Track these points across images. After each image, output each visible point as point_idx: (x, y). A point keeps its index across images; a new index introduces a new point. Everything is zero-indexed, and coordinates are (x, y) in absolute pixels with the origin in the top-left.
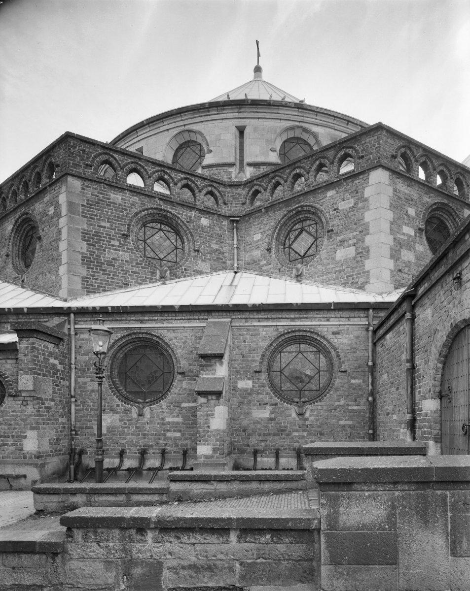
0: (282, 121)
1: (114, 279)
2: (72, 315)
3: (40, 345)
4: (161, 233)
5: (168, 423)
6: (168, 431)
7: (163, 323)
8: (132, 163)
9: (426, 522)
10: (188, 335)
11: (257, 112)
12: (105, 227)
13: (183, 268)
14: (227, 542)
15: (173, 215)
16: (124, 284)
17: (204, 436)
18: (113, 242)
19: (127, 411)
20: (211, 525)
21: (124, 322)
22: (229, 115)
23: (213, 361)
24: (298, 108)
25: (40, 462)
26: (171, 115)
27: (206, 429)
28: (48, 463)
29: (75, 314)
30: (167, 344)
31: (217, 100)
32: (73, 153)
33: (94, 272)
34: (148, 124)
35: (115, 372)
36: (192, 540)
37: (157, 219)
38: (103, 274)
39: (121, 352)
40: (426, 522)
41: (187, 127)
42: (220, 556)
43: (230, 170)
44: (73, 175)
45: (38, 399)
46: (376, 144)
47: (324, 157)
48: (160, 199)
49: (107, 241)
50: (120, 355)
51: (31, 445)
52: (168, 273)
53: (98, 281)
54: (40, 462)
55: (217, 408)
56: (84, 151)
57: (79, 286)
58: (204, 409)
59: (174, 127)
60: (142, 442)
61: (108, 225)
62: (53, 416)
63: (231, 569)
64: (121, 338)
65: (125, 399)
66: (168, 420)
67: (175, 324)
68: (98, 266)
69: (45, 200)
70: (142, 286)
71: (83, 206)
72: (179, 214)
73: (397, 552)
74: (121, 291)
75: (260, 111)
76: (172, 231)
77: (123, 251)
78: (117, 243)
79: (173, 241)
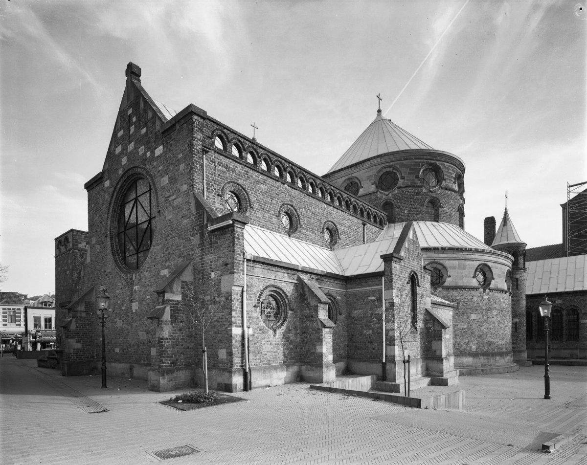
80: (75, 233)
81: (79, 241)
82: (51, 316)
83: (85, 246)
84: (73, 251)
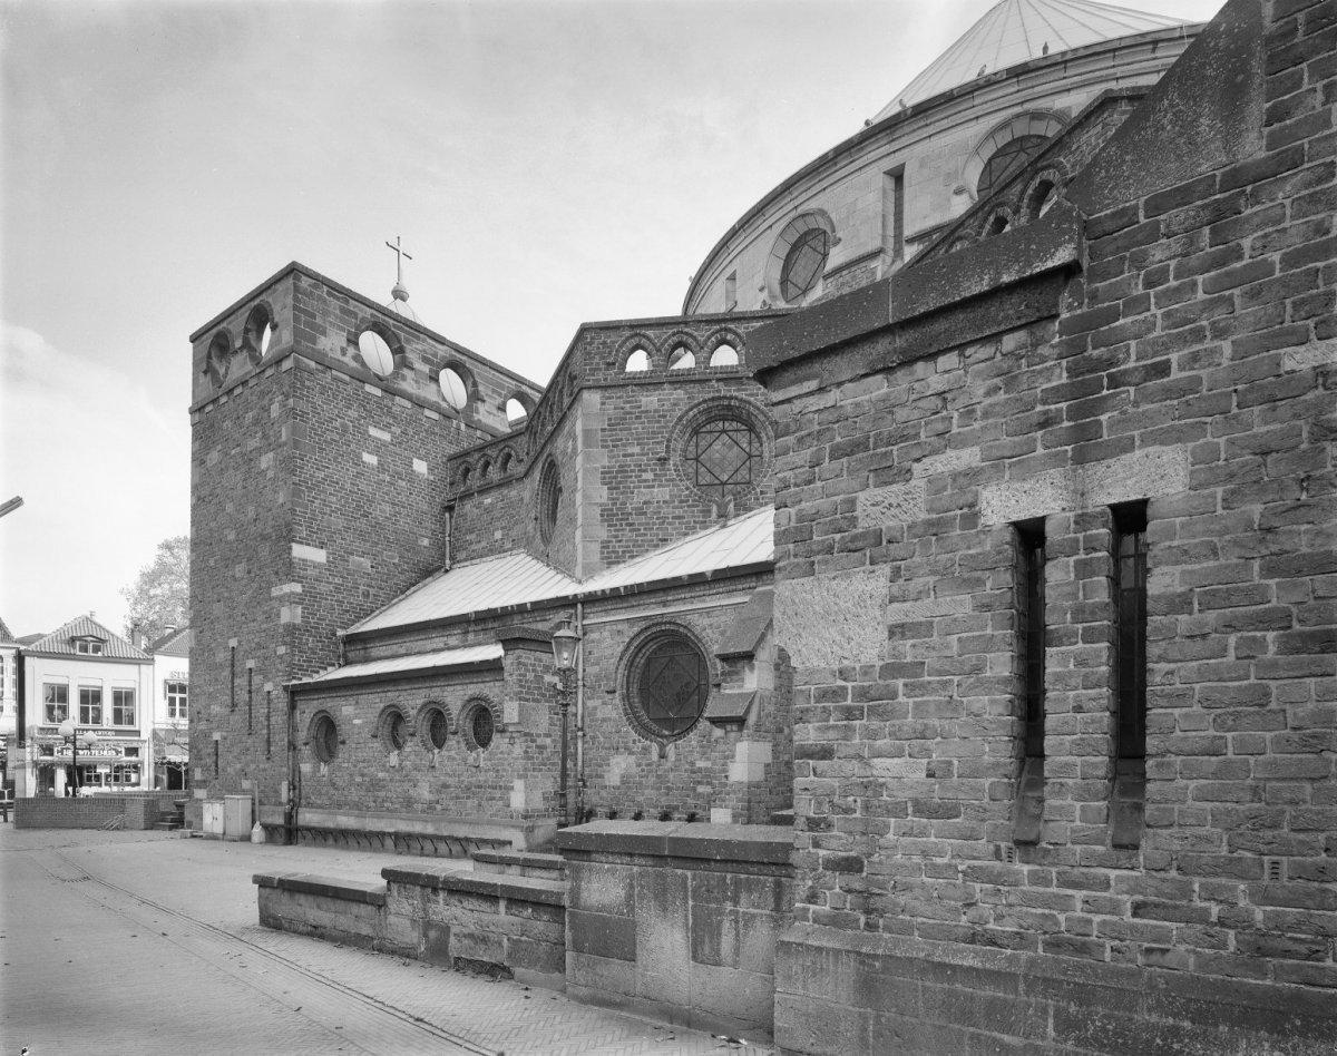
0: (981, 120)
1: (645, 535)
2: (579, 606)
3: (529, 658)
4: (725, 437)
5: (700, 770)
6: (699, 783)
7: (704, 601)
8: (674, 334)
9: (665, 910)
10: (727, 619)
11: (927, 125)
12: (632, 455)
13: (758, 490)
14: (496, 913)
15: (741, 400)
16: (661, 540)
17: (721, 792)
18: (645, 476)
19: (646, 750)
20: (481, 890)
21: (642, 608)
22: (872, 156)
23: (739, 665)
24: (1017, 76)
25: (527, 823)
26: (776, 198)
27: (724, 780)
28: (539, 827)
29: (583, 603)
30: (696, 637)
31: (889, 115)
32: (589, 353)
33: (618, 530)
34: (742, 227)
35: (635, 689)
36: (471, 907)
37: (716, 415)
38: (630, 531)
39: (640, 655)
40: (665, 910)
41: (800, 210)
42: (492, 928)
43: (873, 264)
44: (590, 388)
45: (526, 735)
46: (1100, 141)
47: (1001, 204)
48: (718, 380)
49: (636, 477)
50: (640, 661)
51: (518, 800)
52: (732, 505)
53: (623, 543)
54: (527, 823)
55: (739, 745)
56: (604, 343)
57: (596, 558)
58: (721, 747)
59: (779, 217)
60: (664, 801)
61: (637, 450)
62: (549, 759)
63: (500, 944)
64: (638, 635)
65: (645, 731)
66: (700, 764)
67: (710, 603)
68: (622, 520)
69: (565, 432)
70: (688, 538)
71: (603, 430)
72: (752, 395)
73: (635, 944)
74: (657, 552)
75: (933, 120)
76: (744, 427)
77: (659, 486)
78: (649, 476)
79: (744, 446)
80: (305, 282)
81: (318, 320)
82: (99, 684)
83: (344, 352)
84: (298, 367)
